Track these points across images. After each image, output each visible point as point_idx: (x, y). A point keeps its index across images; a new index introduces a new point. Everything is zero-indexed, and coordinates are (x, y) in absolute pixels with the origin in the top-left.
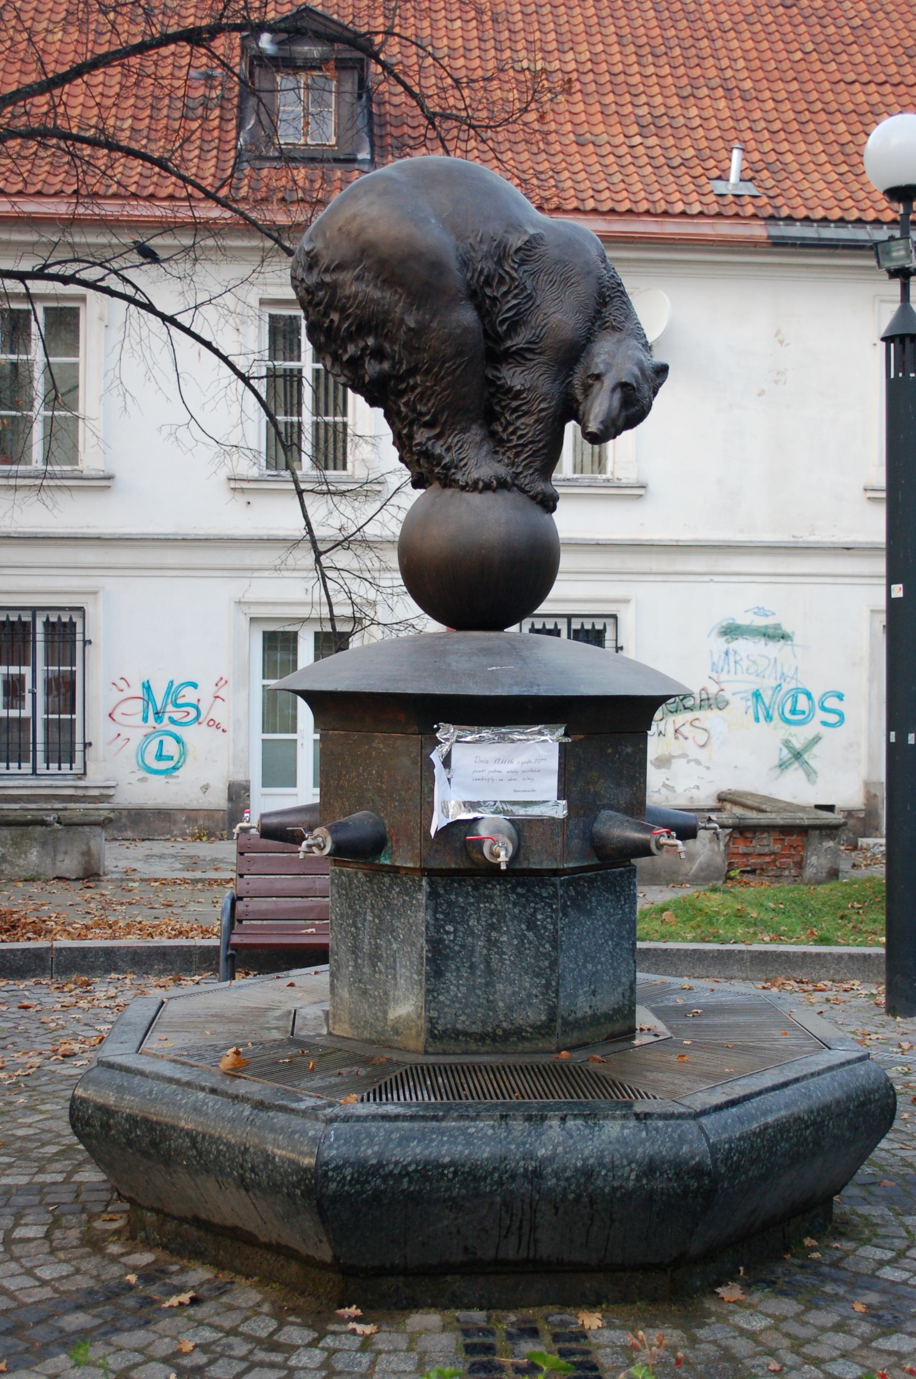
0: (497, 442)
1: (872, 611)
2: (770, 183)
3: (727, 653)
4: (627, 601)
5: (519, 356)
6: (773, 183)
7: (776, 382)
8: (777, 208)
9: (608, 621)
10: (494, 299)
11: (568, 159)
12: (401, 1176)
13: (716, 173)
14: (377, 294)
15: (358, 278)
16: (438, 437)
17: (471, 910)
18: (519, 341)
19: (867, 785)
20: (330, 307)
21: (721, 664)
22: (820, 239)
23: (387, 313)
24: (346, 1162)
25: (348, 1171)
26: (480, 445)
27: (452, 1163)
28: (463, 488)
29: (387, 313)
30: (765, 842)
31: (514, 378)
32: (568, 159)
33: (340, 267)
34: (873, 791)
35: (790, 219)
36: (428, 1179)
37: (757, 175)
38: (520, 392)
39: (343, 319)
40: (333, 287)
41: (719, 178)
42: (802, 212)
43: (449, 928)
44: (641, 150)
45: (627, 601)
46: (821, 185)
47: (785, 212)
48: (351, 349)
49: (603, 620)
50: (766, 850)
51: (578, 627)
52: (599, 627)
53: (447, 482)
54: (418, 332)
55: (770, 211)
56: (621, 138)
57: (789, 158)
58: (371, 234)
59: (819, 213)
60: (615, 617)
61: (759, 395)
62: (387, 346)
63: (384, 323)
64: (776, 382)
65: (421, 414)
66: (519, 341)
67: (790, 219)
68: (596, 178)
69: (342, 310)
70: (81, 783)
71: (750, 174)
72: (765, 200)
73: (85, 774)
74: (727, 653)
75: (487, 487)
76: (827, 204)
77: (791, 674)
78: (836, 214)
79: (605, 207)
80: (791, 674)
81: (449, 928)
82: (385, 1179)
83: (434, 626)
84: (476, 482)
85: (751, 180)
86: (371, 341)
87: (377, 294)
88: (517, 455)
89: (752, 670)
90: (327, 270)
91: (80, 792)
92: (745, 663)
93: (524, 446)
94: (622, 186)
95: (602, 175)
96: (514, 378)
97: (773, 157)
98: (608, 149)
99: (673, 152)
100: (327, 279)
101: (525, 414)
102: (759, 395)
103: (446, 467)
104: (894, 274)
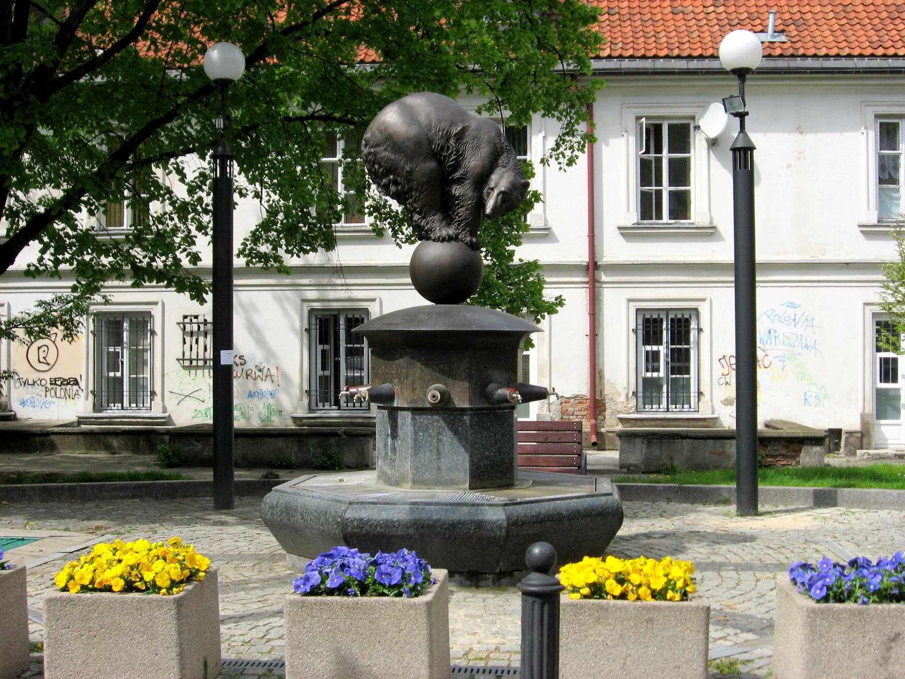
0: (448, 219)
1: (865, 304)
2: (794, 33)
3: (769, 332)
4: (704, 300)
5: (460, 181)
6: (796, 33)
7: (799, 158)
8: (797, 49)
9: (692, 312)
10: (445, 157)
11: (666, 24)
12: (377, 526)
13: (760, 28)
14: (393, 157)
15: (385, 150)
16: (423, 218)
17: (430, 426)
18: (457, 175)
19: (863, 417)
20: (374, 163)
21: (766, 338)
22: (823, 68)
23: (397, 164)
24: (355, 519)
25: (356, 523)
26: (442, 221)
27: (398, 521)
28: (434, 241)
29: (397, 164)
30: (776, 448)
31: (456, 190)
32: (666, 24)
33: (377, 145)
34: (866, 420)
35: (804, 56)
36: (387, 526)
37: (787, 29)
38: (459, 197)
39: (380, 167)
40: (375, 154)
41: (762, 31)
42: (812, 52)
43: (421, 434)
44: (713, 15)
45: (704, 300)
46: (828, 33)
47: (801, 52)
48: (384, 181)
49: (689, 312)
50: (777, 453)
51: (673, 317)
52: (686, 316)
53: (428, 238)
54: (410, 173)
55: (791, 51)
56: (701, 8)
57: (809, 16)
58: (390, 130)
59: (824, 51)
60: (696, 310)
61: (788, 167)
62: (399, 179)
63: (396, 169)
64: (799, 158)
65: (415, 208)
66: (457, 175)
67: (804, 56)
68: (682, 35)
69: (379, 164)
70: (368, 415)
71: (782, 27)
72: (789, 44)
73: (369, 409)
74: (769, 332)
75: (443, 240)
76: (830, 46)
77: (812, 344)
78: (834, 52)
79: (685, 54)
80: (812, 344)
81: (421, 434)
82: (370, 526)
83: (429, 303)
84: (439, 238)
85: (782, 31)
86: (391, 177)
87: (393, 157)
88: (459, 225)
89: (786, 342)
90: (372, 147)
91: (366, 421)
92: (781, 338)
93: (461, 221)
94: (698, 39)
95: (686, 33)
96: (456, 190)
97: (798, 16)
98: (692, 15)
99: (733, 16)
100: (372, 150)
101: (462, 206)
102: (788, 167)
103: (427, 231)
104: (736, 115)
